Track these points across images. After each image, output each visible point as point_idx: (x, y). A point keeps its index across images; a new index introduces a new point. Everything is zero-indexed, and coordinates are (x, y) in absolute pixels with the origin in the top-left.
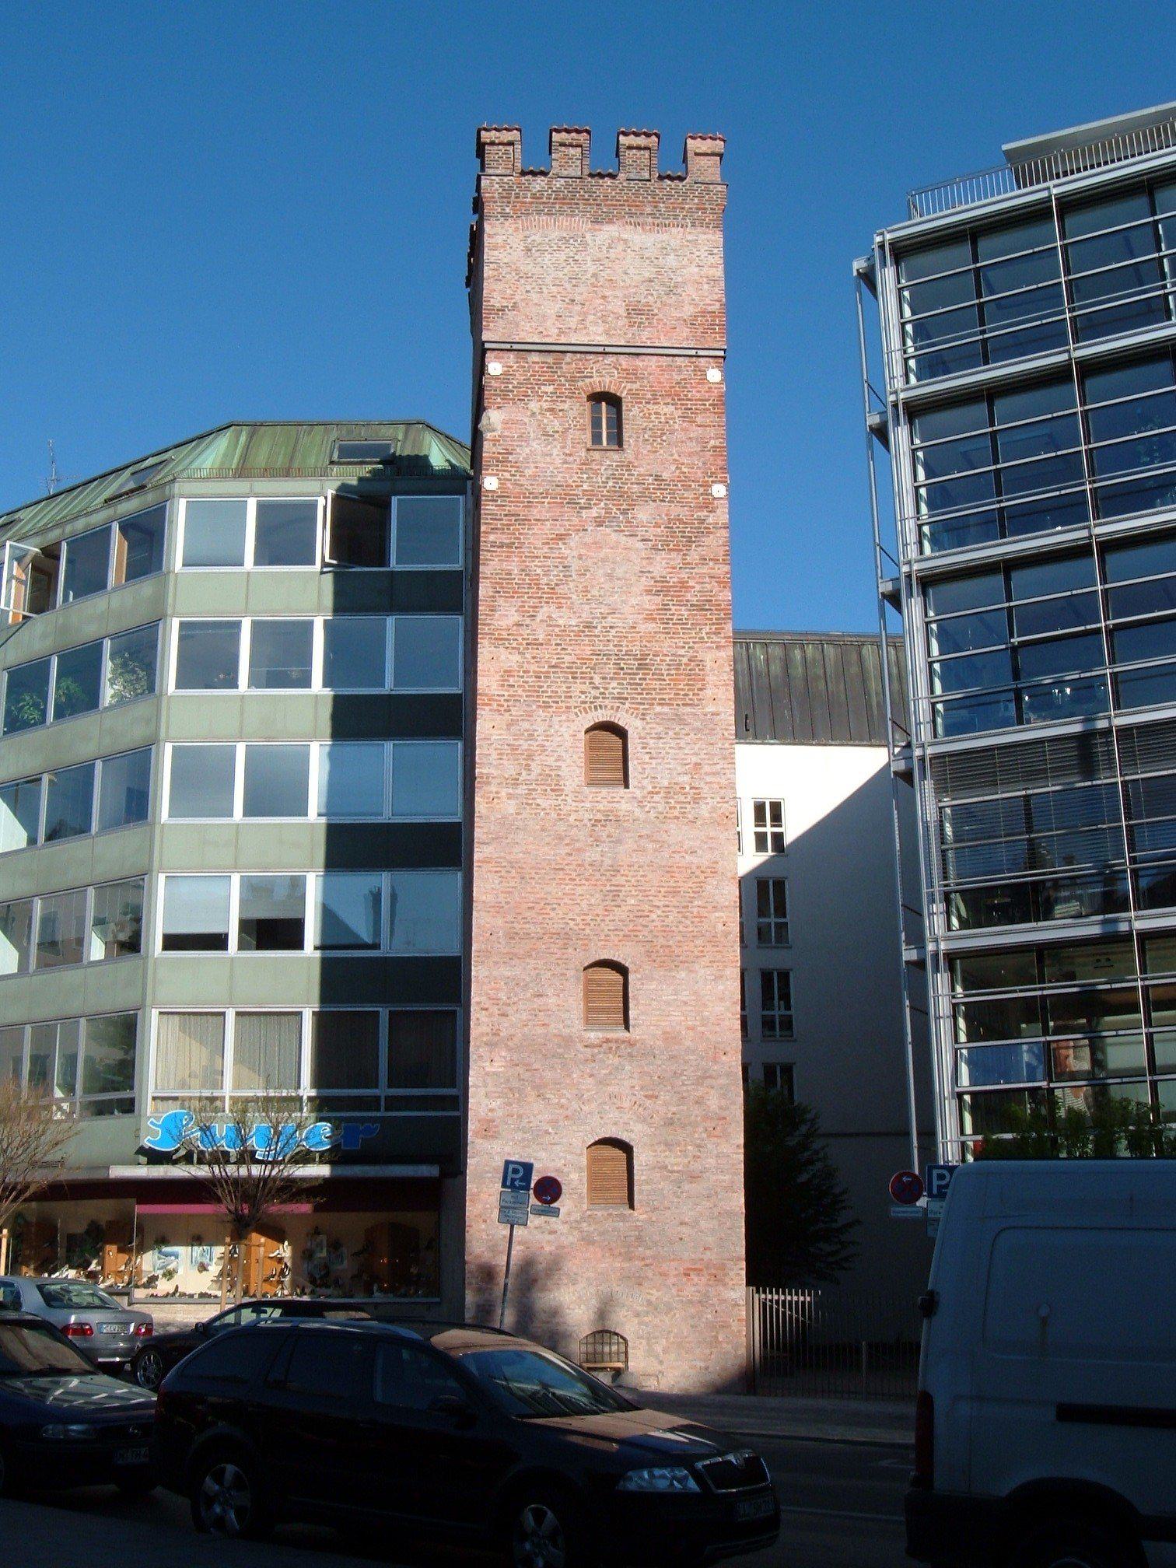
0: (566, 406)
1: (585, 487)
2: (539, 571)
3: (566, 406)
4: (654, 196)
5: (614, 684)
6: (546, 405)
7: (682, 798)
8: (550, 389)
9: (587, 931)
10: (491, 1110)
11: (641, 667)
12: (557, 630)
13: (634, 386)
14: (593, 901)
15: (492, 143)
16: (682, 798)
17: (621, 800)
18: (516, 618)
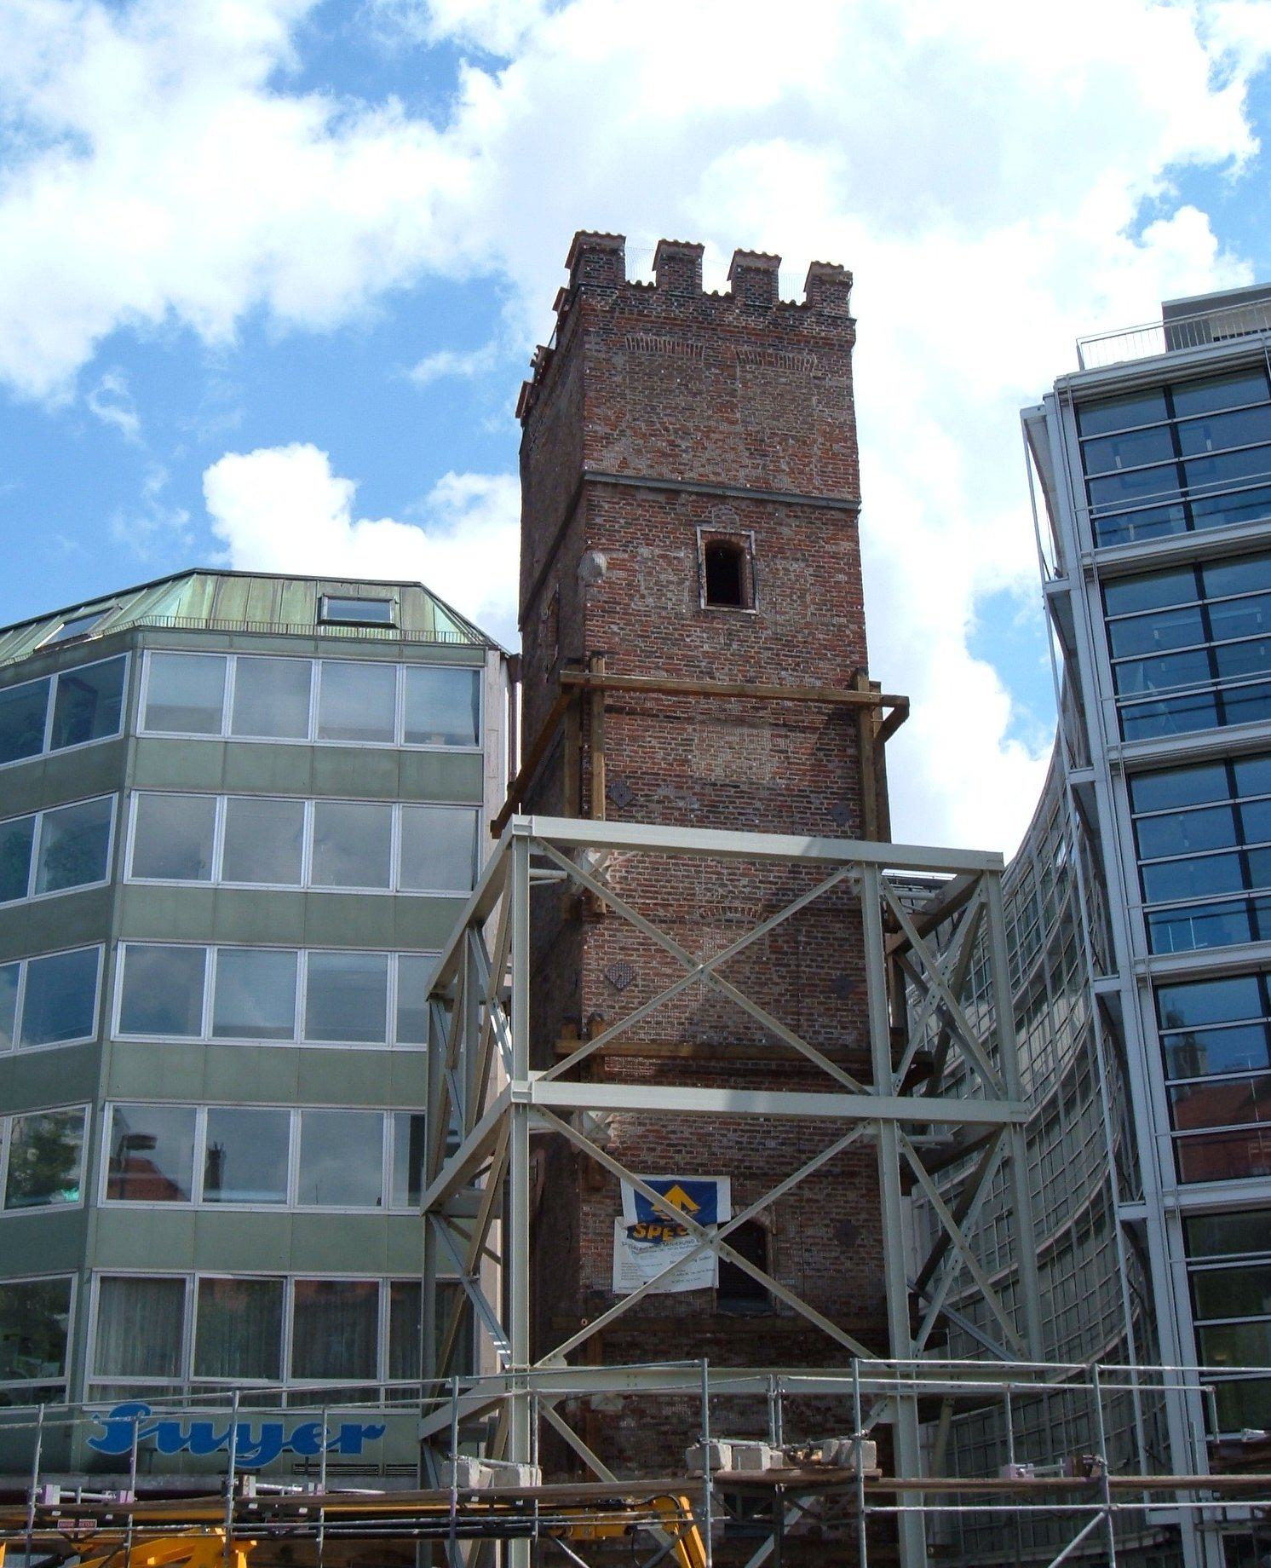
1: (706, 647)
6: (657, 552)
12: (676, 813)
16: (826, 1021)
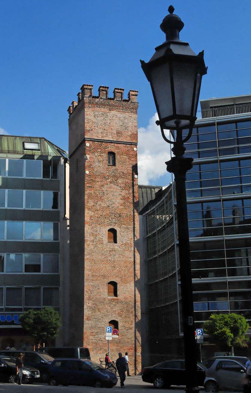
0: (103, 155)
1: (108, 174)
2: (98, 193)
3: (103, 155)
4: (122, 105)
5: (114, 220)
6: (99, 154)
7: (128, 246)
8: (100, 150)
9: (109, 275)
10: (89, 314)
11: (120, 216)
12: (102, 207)
13: (118, 151)
14: (110, 268)
15: (86, 89)
16: (128, 246)
17: (116, 246)
18: (93, 204)
